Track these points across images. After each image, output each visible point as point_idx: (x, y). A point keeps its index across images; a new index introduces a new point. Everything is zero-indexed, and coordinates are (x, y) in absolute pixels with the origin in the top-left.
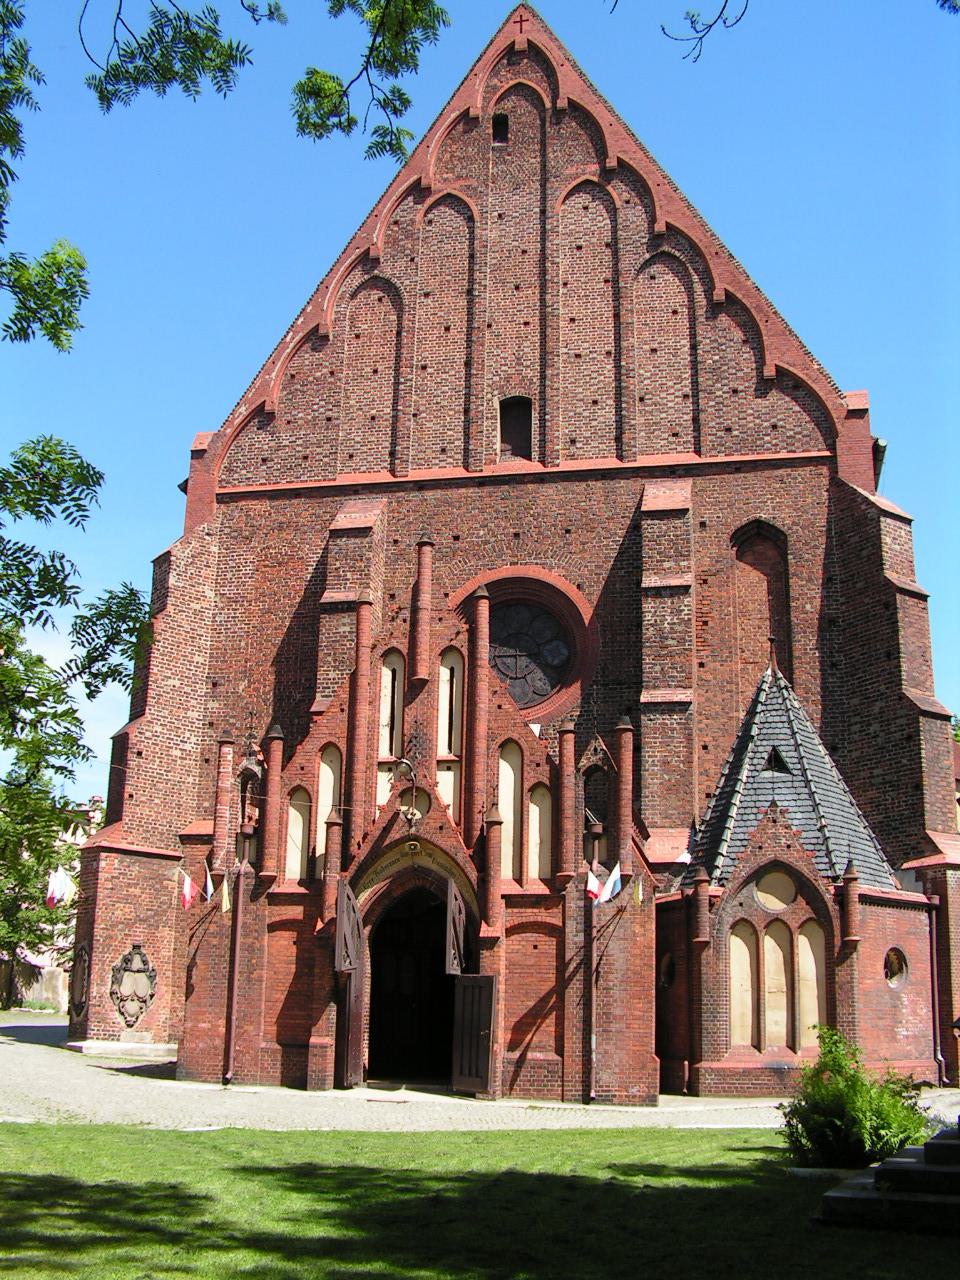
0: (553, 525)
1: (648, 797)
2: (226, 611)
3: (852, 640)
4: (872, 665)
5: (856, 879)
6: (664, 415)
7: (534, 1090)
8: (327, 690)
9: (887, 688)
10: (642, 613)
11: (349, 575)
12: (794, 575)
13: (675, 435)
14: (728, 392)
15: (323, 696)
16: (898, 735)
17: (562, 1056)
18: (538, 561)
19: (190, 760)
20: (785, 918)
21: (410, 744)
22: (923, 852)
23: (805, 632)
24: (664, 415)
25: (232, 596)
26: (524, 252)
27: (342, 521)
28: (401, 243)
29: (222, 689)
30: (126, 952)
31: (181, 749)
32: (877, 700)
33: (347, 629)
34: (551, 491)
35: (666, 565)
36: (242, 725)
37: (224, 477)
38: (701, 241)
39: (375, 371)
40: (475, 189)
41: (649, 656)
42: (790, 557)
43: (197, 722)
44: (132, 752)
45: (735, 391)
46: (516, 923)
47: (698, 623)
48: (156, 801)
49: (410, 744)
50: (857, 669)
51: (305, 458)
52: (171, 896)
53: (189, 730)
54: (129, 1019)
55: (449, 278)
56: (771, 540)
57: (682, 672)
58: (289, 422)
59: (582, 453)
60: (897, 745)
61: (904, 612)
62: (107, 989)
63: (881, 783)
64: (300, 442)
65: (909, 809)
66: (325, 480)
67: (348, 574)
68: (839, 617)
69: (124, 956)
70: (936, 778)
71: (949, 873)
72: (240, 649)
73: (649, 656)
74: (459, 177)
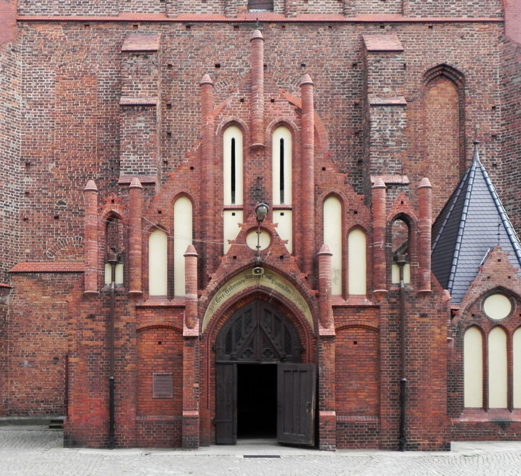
2: (33, 111)
7: (358, 442)
8: (128, 169)
11: (140, 86)
15: (125, 173)
17: (379, 418)
18: (281, 86)
19: (13, 219)
20: (504, 325)
25: (37, 100)
27: (131, 45)
29: (34, 168)
31: (5, 211)
34: (290, 36)
37: (22, 7)
42: (466, 91)
43: (16, 192)
50: (512, 169)
52: (5, 315)
53: (10, 197)
57: (399, 164)
59: (313, 9)
66: (109, 15)
67: (139, 85)
68: (499, 134)
72: (47, 140)
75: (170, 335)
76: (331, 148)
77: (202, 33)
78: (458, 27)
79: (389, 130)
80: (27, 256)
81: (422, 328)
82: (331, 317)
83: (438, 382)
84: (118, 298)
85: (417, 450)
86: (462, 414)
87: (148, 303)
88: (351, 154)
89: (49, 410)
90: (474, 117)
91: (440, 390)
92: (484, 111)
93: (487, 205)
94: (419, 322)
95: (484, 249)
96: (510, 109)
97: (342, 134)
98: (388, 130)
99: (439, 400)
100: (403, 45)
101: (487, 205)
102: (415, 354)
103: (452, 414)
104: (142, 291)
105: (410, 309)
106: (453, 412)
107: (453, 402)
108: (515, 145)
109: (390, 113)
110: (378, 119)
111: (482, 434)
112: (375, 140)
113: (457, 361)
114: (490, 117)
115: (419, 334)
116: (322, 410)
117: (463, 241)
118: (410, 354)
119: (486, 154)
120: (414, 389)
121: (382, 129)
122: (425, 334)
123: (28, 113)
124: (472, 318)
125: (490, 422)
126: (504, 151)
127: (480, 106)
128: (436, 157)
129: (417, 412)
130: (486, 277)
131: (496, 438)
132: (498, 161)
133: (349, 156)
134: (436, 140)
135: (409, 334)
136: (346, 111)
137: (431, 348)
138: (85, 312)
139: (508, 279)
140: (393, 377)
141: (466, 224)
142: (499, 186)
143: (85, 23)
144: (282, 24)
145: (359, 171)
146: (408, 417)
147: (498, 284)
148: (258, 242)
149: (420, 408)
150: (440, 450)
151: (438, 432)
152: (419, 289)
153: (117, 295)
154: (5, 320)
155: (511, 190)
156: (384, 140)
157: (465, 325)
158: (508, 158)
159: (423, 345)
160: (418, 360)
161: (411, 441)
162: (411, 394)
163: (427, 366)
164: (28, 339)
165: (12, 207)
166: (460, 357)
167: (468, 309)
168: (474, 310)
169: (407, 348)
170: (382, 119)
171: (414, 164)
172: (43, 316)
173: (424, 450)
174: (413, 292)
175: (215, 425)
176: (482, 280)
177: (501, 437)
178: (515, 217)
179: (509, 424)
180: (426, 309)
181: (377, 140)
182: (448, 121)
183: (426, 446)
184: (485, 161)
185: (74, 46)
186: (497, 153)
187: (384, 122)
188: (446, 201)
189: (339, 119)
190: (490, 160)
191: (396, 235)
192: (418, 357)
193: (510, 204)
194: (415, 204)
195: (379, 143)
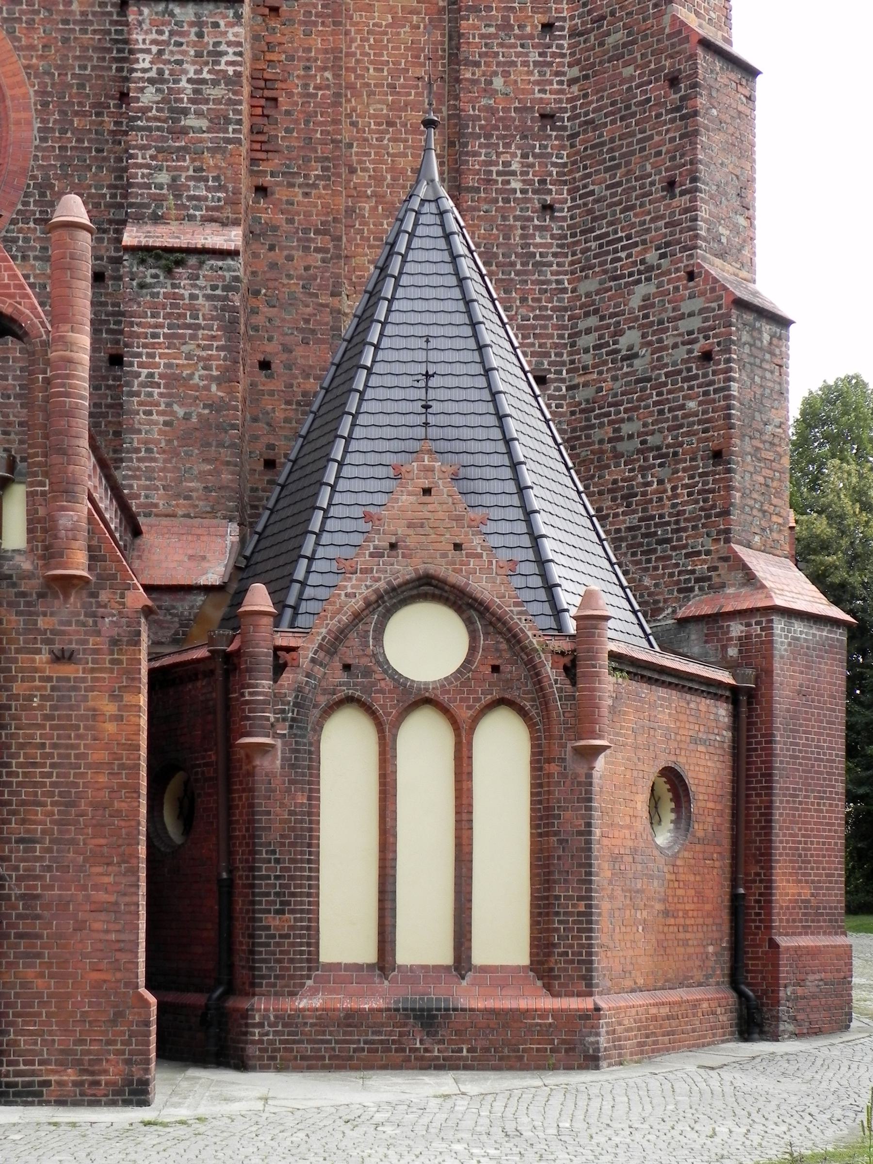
1: (137, 450)
4: (633, 207)
5: (607, 618)
9: (663, 256)
10: (131, 52)
16: (681, 353)
20: (444, 698)
22: (723, 586)
23: (488, 136)
32: (638, 282)
41: (143, 148)
47: (255, 102)
50: (594, 220)
57: (220, 188)
60: (680, 372)
61: (710, 95)
63: (639, 452)
65: (696, 502)
68: (565, 110)
70: (756, 443)
71: (779, 625)
73: (143, 148)
76: (43, 139)
79: (189, 81)
81: (60, 699)
83: (111, 879)
85: (40, 1103)
86: (309, 983)
88: (105, 159)
90: (486, 54)
91: (116, 904)
92: (517, 37)
93: (443, 319)
94: (49, 679)
96: (593, 29)
97: (79, 94)
98: (184, 78)
99: (113, 937)
101: (443, 319)
102: (35, 784)
103: (274, 985)
105: (18, 633)
106: (277, 977)
107: (278, 944)
108: (603, 144)
109: (192, 24)
110: (154, 42)
111: (363, 1049)
112: (146, 110)
113: (291, 813)
114: (534, 56)
115: (46, 717)
117: (358, 432)
118: (19, 784)
119: (524, 173)
120: (29, 898)
121: (166, 76)
122: (69, 717)
124: (343, 678)
125: (388, 1009)
126: (574, 163)
127: (506, 19)
128: (378, 179)
129: (41, 975)
130: (386, 544)
131: (408, 1060)
132: (558, 194)
133: (100, 168)
134: (378, 124)
135: (14, 718)
136: (91, 23)
137: (89, 766)
139: (452, 553)
141: (373, 377)
142: (558, 273)
147: (422, 569)
149: (50, 965)
150: (113, 1103)
151: (109, 1043)
152: (47, 566)
155: (590, 285)
156: (172, 110)
157: (323, 700)
158: (585, 186)
159: (60, 756)
160: (43, 804)
161: (18, 1074)
162: (19, 916)
163: (76, 823)
166: (302, 799)
167: (333, 644)
168: (350, 653)
169: (8, 765)
170: (168, 43)
171: (300, 198)
173: (61, 1103)
174: (29, 576)
176: (372, 555)
177: (422, 1058)
178: (600, 373)
179: (448, 1017)
180: (74, 637)
181: (150, 109)
182: (414, 64)
183: (70, 1088)
184: (519, 195)
186: (555, 171)
187: (172, 53)
189: (71, 48)
190: (535, 192)
191: (199, 415)
192: (44, 794)
193: (588, 331)
194: (302, 324)
195: (157, 119)
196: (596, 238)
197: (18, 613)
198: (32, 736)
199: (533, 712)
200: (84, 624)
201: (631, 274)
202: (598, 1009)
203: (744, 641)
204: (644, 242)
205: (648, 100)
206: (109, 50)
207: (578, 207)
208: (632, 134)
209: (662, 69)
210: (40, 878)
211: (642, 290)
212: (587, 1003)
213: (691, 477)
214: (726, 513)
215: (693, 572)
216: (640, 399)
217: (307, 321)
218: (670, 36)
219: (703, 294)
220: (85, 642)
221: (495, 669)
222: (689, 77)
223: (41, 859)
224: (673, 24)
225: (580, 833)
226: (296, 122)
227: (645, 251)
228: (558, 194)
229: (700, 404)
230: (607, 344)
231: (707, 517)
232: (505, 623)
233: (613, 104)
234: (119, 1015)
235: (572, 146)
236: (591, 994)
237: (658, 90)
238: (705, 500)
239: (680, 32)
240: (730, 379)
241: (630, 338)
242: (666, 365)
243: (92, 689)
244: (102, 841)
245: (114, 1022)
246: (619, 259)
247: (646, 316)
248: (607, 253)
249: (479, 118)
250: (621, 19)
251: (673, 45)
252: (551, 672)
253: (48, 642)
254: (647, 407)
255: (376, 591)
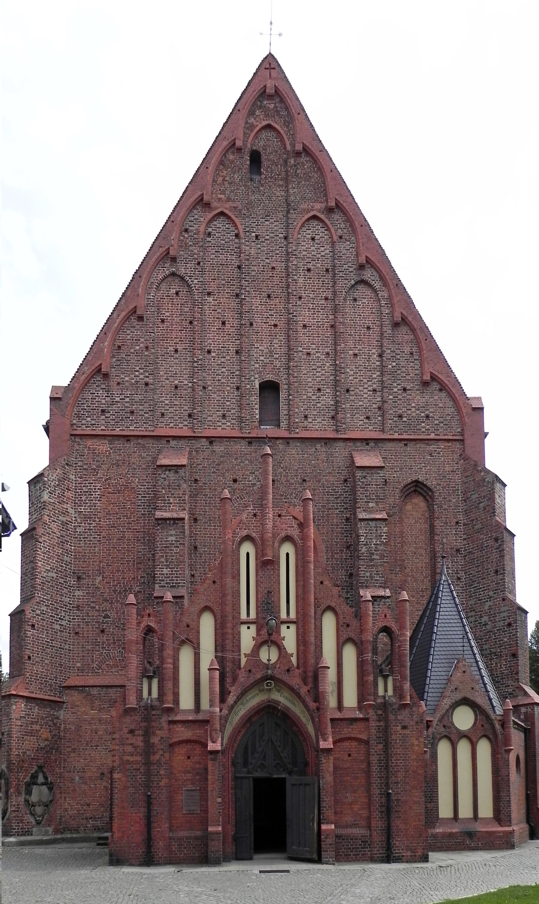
0: (295, 476)
3: (471, 562)
4: (485, 578)
6: (361, 403)
7: (354, 855)
9: (495, 593)
12: (438, 518)
13: (368, 418)
14: (401, 390)
15: (160, 587)
16: (502, 623)
20: (469, 735)
21: (268, 605)
22: (517, 696)
24: (361, 403)
26: (273, 268)
28: (191, 248)
29: (84, 581)
30: (33, 772)
32: (487, 601)
33: (174, 538)
35: (371, 505)
36: (99, 608)
38: (387, 274)
39: (176, 351)
40: (240, 211)
41: (363, 565)
44: (28, 625)
45: (405, 390)
46: (338, 738)
48: (46, 661)
49: (268, 605)
50: (472, 582)
51: (132, 412)
52: (59, 730)
54: (38, 819)
55: (223, 282)
56: (422, 495)
57: (382, 577)
58: (118, 384)
60: (501, 629)
62: (22, 799)
63: (489, 654)
64: (127, 400)
65: (508, 670)
69: (32, 774)
72: (95, 553)
73: (363, 565)
74: (229, 200)
75: (197, 749)
76: (327, 562)
77: (222, 449)
78: (428, 444)
80: (78, 670)
81: (404, 740)
82: (329, 729)
84: (154, 712)
85: (402, 862)
86: (437, 824)
87: (178, 718)
88: (343, 567)
89: (97, 826)
91: (419, 801)
93: (453, 617)
95: (452, 661)
99: (419, 811)
100: (384, 462)
101: (453, 617)
103: (429, 825)
104: (174, 705)
108: (475, 559)
113: (433, 772)
115: (401, 746)
116: (323, 823)
118: (395, 766)
123: (80, 526)
124: (443, 729)
126: (466, 564)
128: (412, 570)
129: (401, 823)
132: (462, 574)
133: (342, 570)
137: (411, 760)
138: (126, 727)
140: (381, 789)
143: (127, 438)
144: (287, 440)
145: (351, 583)
146: (394, 829)
147: (464, 695)
148: (268, 655)
150: (420, 862)
152: (401, 701)
153: (154, 709)
154: (59, 735)
156: (370, 553)
157: (438, 736)
160: (400, 772)
162: (396, 806)
163: (408, 777)
164: (79, 754)
165: (65, 620)
171: (394, 577)
172: (91, 731)
173: (407, 862)
175: (235, 841)
176: (451, 692)
179: (475, 834)
183: (409, 857)
185: (118, 460)
186: (460, 567)
188: (420, 613)
193: (472, 616)
195: (366, 556)
196: (473, 588)
197: (393, 715)
198: (397, 751)
199: (493, 739)
200: (409, 717)
201: (485, 599)
202: (514, 830)
203: (526, 714)
204: (489, 589)
205: (489, 545)
206: (344, 534)
207: (467, 578)
208: (484, 556)
209: (493, 536)
210: (400, 794)
211: (488, 604)
212: (510, 829)
213: (506, 662)
214: (517, 673)
215: (507, 692)
216: (489, 638)
217: (397, 615)
218: (495, 526)
219: (508, 605)
220: (409, 723)
221: (482, 726)
222: (501, 539)
223: (400, 788)
224: (496, 523)
225: (507, 776)
226: (393, 554)
227: (489, 592)
228: (462, 574)
229: (508, 639)
230: (478, 621)
231: (512, 674)
232: (485, 712)
233: (477, 546)
234: (421, 834)
235: (465, 559)
236: (511, 826)
237: (491, 542)
238: (511, 669)
239: (498, 525)
240: (517, 632)
241: (485, 619)
242: (497, 627)
243: (411, 737)
244: (415, 783)
245: (419, 837)
246: (481, 594)
247: (490, 612)
248: (477, 592)
249: (440, 551)
250: (479, 520)
251: (496, 529)
252: (498, 726)
253: (400, 723)
254: (491, 640)
255: (452, 703)
